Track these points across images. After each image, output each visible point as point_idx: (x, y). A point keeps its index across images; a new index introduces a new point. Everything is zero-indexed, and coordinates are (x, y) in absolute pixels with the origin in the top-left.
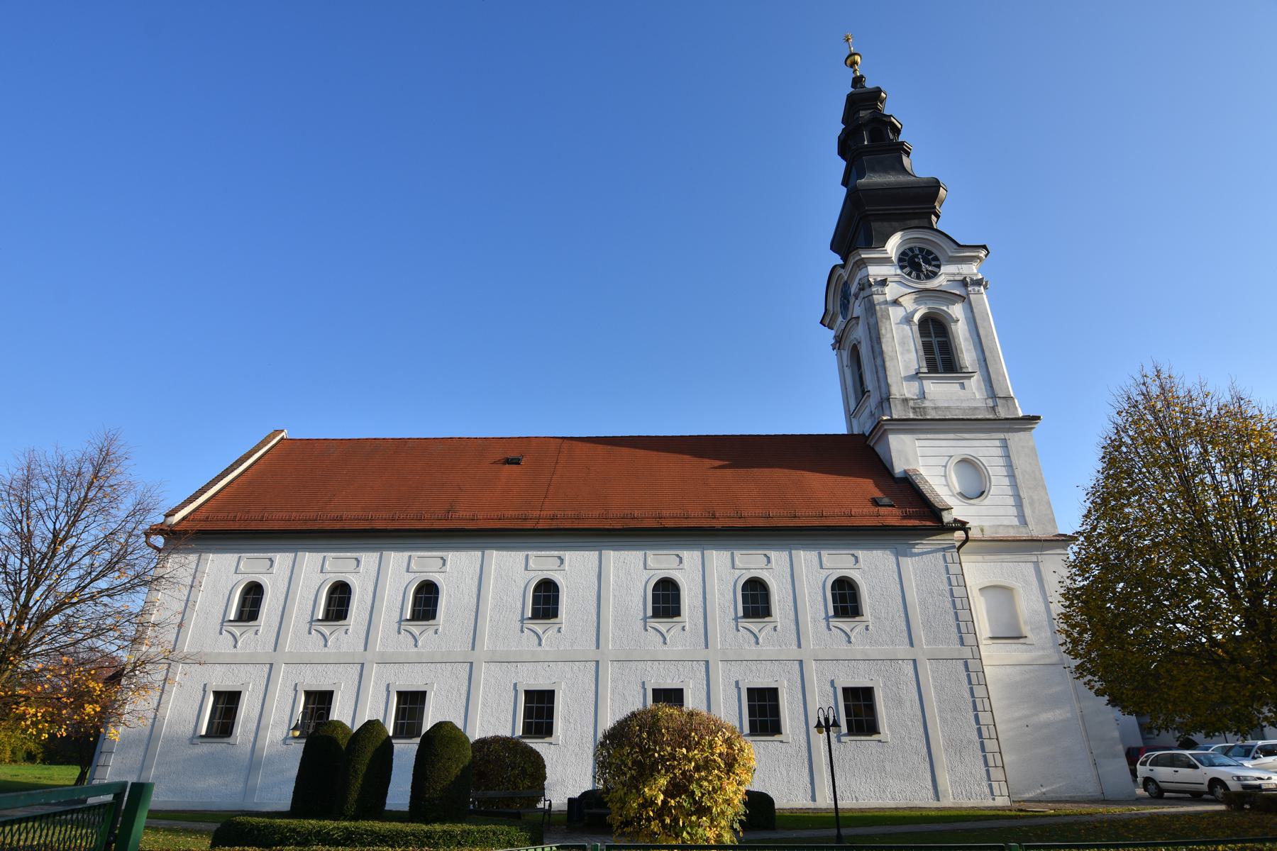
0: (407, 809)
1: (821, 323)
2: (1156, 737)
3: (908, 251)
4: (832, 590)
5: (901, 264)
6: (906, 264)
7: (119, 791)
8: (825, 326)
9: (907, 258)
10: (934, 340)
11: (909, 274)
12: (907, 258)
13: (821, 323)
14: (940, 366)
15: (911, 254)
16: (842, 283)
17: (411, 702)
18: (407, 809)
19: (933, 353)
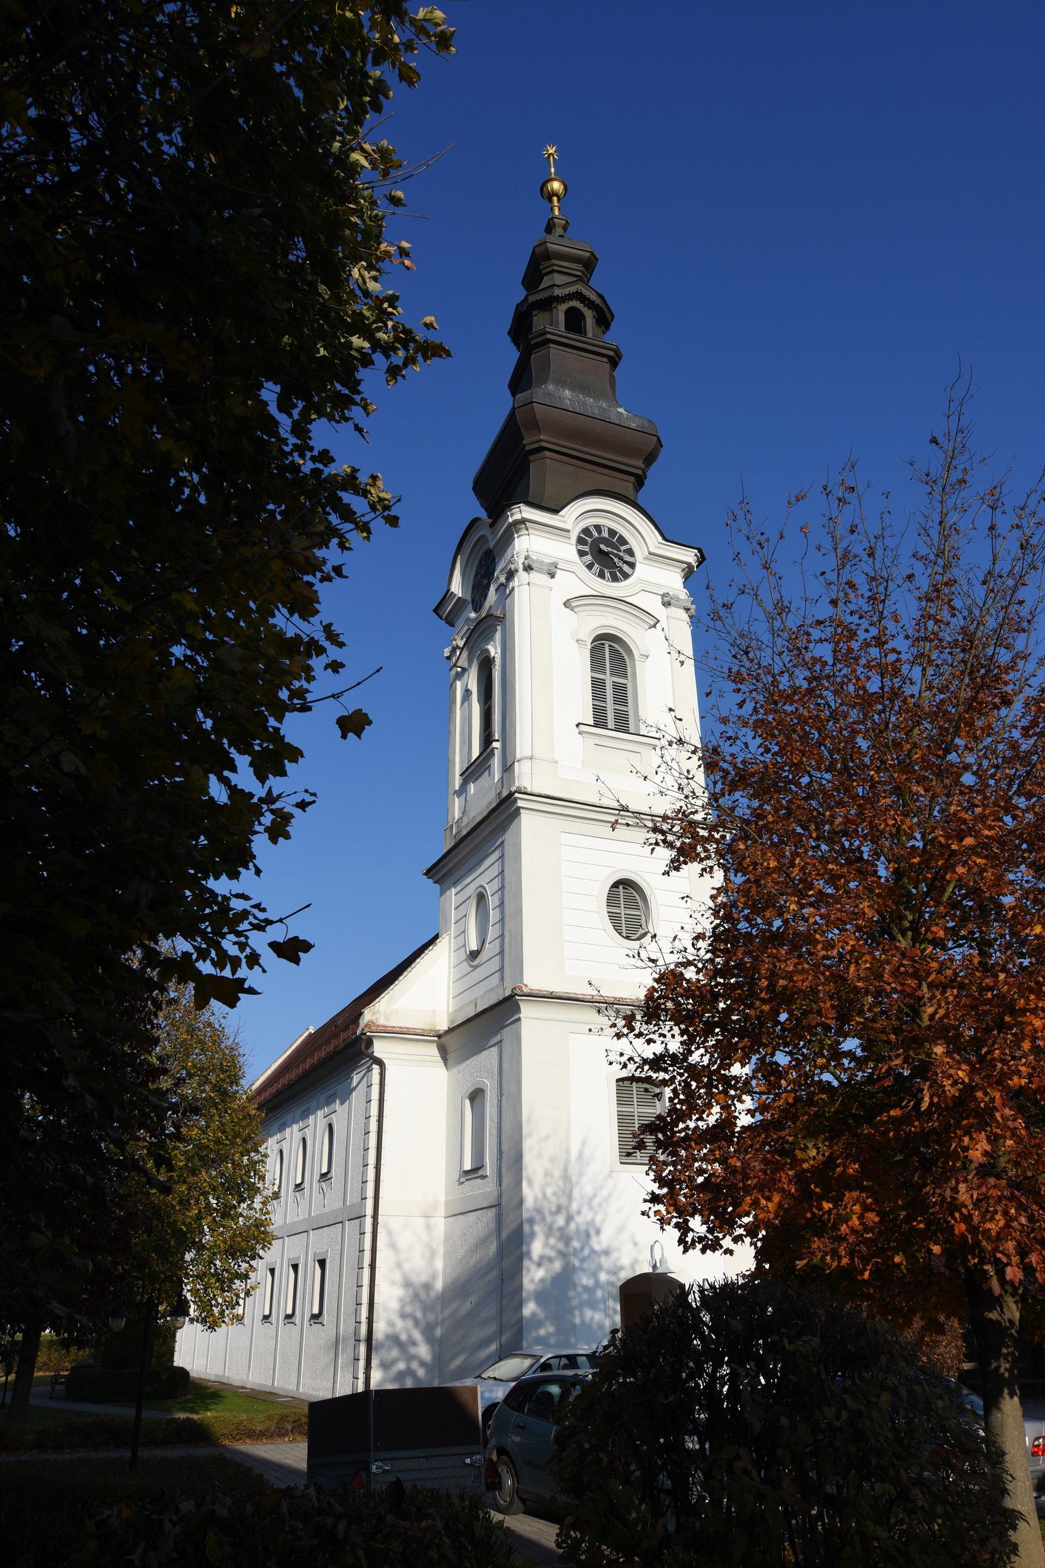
0: (175, 1364)
1: (436, 611)
2: (268, 957)
3: (592, 529)
4: (621, 536)
5: (580, 547)
6: (586, 548)
7: (433, 1051)
8: (441, 618)
9: (590, 540)
10: (609, 680)
11: (590, 567)
12: (590, 540)
13: (436, 611)
14: (611, 723)
15: (596, 534)
16: (483, 550)
17: (754, 738)
18: (175, 1364)
19: (616, 685)
